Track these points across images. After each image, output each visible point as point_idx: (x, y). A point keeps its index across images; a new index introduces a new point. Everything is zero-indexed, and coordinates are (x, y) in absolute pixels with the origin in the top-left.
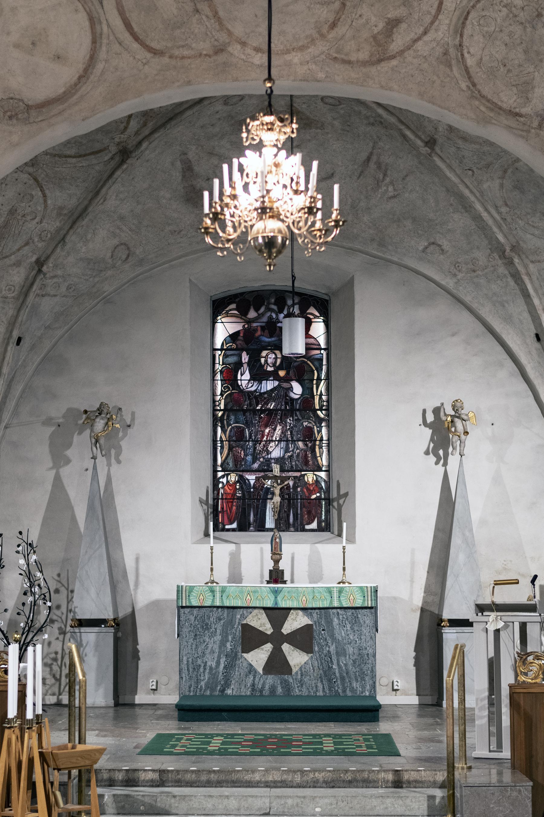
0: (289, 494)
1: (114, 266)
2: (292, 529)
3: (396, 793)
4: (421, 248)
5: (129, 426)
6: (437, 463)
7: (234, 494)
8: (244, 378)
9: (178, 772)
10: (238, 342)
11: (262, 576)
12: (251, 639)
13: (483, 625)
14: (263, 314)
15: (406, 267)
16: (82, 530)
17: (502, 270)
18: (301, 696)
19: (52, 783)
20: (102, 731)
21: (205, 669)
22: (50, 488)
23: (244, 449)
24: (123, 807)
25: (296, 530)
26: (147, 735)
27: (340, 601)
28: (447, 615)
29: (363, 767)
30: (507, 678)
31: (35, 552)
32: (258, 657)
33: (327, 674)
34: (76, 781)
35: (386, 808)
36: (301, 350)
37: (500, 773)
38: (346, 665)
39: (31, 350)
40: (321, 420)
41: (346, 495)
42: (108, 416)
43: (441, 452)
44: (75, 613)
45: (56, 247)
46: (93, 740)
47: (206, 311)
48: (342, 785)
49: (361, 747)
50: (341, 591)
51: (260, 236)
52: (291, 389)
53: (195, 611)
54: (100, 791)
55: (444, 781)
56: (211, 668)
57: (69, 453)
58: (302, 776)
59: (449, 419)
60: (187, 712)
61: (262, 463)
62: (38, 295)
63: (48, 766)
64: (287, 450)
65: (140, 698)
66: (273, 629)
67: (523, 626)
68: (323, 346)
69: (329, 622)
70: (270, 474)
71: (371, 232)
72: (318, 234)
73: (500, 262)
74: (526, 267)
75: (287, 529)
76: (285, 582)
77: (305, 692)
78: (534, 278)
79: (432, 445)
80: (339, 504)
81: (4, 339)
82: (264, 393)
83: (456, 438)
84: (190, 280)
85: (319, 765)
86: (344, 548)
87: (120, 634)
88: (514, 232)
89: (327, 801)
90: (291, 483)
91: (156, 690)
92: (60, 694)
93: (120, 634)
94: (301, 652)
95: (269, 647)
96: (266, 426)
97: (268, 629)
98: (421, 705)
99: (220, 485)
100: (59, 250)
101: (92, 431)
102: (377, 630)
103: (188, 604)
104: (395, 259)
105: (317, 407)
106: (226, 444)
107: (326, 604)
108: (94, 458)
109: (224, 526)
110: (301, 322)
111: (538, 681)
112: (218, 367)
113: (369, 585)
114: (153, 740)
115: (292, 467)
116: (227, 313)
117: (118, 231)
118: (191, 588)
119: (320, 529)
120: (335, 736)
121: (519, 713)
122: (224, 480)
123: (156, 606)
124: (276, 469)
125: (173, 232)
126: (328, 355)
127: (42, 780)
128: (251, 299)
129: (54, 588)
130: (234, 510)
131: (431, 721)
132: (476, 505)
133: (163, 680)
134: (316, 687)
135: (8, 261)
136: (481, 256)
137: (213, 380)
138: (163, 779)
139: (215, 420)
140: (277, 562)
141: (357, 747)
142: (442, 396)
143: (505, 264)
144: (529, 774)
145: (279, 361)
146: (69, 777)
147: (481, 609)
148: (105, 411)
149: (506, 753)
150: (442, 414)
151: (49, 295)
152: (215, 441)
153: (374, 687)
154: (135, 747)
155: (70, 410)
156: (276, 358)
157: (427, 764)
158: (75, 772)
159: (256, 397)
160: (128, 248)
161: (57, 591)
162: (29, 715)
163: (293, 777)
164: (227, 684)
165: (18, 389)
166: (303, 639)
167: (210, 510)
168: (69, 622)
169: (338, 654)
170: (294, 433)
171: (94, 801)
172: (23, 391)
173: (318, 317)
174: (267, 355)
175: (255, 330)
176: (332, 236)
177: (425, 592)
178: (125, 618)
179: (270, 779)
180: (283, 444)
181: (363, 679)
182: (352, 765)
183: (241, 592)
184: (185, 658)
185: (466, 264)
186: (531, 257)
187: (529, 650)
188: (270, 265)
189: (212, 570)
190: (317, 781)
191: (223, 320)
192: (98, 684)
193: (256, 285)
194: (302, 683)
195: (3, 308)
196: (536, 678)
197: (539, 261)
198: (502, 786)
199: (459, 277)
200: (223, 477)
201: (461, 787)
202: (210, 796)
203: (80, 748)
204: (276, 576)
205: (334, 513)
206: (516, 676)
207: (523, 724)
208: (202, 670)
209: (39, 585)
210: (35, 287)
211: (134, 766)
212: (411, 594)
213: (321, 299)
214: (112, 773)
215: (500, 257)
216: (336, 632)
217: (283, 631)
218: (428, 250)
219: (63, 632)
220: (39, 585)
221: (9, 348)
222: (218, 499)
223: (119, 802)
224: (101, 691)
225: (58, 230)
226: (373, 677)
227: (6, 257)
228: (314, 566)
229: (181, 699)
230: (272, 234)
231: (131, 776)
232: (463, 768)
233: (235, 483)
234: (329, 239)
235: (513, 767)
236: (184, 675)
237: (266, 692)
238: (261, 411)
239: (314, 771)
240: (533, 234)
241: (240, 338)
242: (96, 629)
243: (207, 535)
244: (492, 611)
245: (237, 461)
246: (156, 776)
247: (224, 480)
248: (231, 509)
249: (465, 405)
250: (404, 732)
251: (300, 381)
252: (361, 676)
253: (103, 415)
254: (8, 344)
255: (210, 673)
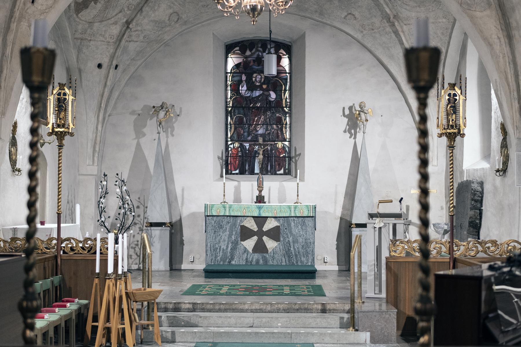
0: (268, 154)
1: (170, 25)
2: (269, 173)
3: (323, 315)
4: (343, 16)
5: (178, 115)
6: (350, 137)
7: (237, 154)
8: (243, 89)
9: (203, 304)
10: (240, 69)
11: (252, 199)
12: (246, 233)
13: (372, 225)
14: (254, 53)
15: (335, 27)
16: (152, 173)
17: (388, 29)
18: (273, 265)
19: (133, 309)
20: (162, 283)
21: (220, 250)
22: (134, 150)
23: (243, 129)
24: (172, 323)
25: (272, 174)
26: (187, 285)
27: (295, 213)
28: (354, 221)
29: (305, 302)
30: (385, 254)
31: (125, 185)
32: (250, 244)
33: (288, 253)
34: (146, 308)
35: (317, 324)
36: (274, 72)
37: (380, 305)
38: (298, 248)
39: (124, 72)
40: (286, 113)
41: (300, 155)
42: (167, 110)
43: (353, 131)
44: (148, 219)
45: (138, 13)
46: (155, 287)
47: (223, 51)
48: (293, 311)
49: (304, 291)
50: (295, 208)
51: (248, 5)
52: (270, 95)
53: (215, 218)
54: (159, 314)
55: (349, 309)
56: (223, 250)
57: (145, 130)
58: (271, 307)
59: (357, 112)
60: (210, 273)
61: (253, 136)
62: (127, 41)
63: (131, 300)
64: (267, 130)
65: (183, 267)
66: (258, 230)
67: (394, 226)
68: (288, 71)
69: (289, 225)
70: (257, 143)
71: (316, 7)
72: (281, 4)
73: (387, 24)
74: (402, 27)
75: (267, 174)
76: (265, 203)
77: (275, 263)
78: (406, 33)
79: (348, 127)
80: (295, 160)
81: (108, 66)
82: (255, 98)
83: (361, 123)
84: (213, 33)
85: (280, 301)
86: (298, 184)
87: (173, 231)
88: (396, 8)
89: (284, 319)
90: (269, 148)
91: (193, 262)
92: (140, 264)
93: (173, 231)
94: (273, 241)
95: (255, 238)
96: (256, 116)
97: (255, 228)
98: (340, 271)
99: (230, 149)
100: (139, 15)
101: (157, 118)
102: (315, 229)
103: (211, 214)
104: (328, 22)
105: (284, 106)
106: (233, 126)
107: (287, 215)
108: (159, 133)
109: (232, 171)
110: (274, 57)
111: (402, 255)
112: (229, 83)
113: (311, 204)
114: (190, 287)
115: (270, 139)
116: (234, 52)
117: (172, 5)
118: (213, 206)
119: (285, 174)
120: (291, 286)
121: (391, 273)
122: (232, 146)
123: (193, 215)
124: (261, 140)
125: (203, 6)
126: (290, 76)
127: (127, 308)
128: (247, 45)
129: (137, 205)
130: (237, 163)
131: (344, 278)
132: (371, 161)
133: (197, 256)
134: (282, 260)
135: (110, 22)
136: (377, 21)
137: (226, 90)
138: (194, 308)
139: (227, 113)
140: (260, 191)
141: (303, 291)
142: (353, 99)
143: (390, 26)
144: (396, 306)
145: (263, 80)
146: (142, 306)
147: (372, 216)
148: (165, 107)
149: (384, 295)
150: (353, 110)
151: (133, 41)
152: (226, 124)
153: (313, 260)
154: (180, 291)
155: (145, 106)
156: (261, 78)
157: (340, 300)
158: (145, 303)
159: (250, 100)
160: (178, 15)
161: (138, 207)
162: (120, 272)
163: (266, 307)
164: (232, 258)
165: (116, 94)
166: (275, 234)
167: (224, 163)
168: (145, 224)
169: (293, 242)
170: (271, 120)
171: (156, 319)
172: (119, 96)
173: (285, 55)
174: (256, 76)
175: (250, 62)
176: (289, 5)
177: (343, 209)
178: (176, 222)
179: (254, 308)
180: (265, 126)
181: (307, 256)
182: (299, 301)
183: (240, 208)
184: (209, 244)
185: (368, 25)
186: (404, 22)
187: (397, 239)
188: (254, 21)
189: (224, 195)
190: (279, 309)
191: (232, 56)
192: (161, 258)
193: (251, 36)
194: (273, 258)
195: (108, 48)
196: (400, 253)
197: (409, 24)
198: (381, 312)
199: (364, 33)
200: (231, 144)
201: (358, 313)
202: (221, 317)
203: (148, 290)
204: (260, 199)
205: (293, 165)
206: (390, 252)
207: (393, 279)
208: (218, 250)
209: (128, 204)
210: (125, 36)
211: (178, 301)
212: (335, 210)
213: (287, 45)
214: (166, 305)
215: (387, 22)
216: (293, 230)
217: (263, 229)
218: (347, 18)
219: (141, 230)
220: (128, 204)
221: (111, 71)
222: (228, 157)
223: (171, 320)
224: (163, 262)
225: (139, 4)
226: (313, 254)
227: (109, 19)
228: (280, 194)
229: (206, 266)
230: (255, 4)
231: (177, 306)
232: (359, 303)
233: (238, 148)
234: (287, 7)
235: (387, 302)
236: (208, 253)
237: (254, 263)
238: (253, 108)
239: (278, 304)
240: (406, 9)
241: (241, 66)
242: (160, 228)
243: (222, 176)
244: (377, 217)
245: (239, 135)
246: (190, 306)
247: (232, 146)
248: (235, 163)
249: (366, 105)
250: (331, 287)
251: (275, 91)
252: (307, 254)
253: (164, 109)
254: (110, 69)
255: (223, 252)
